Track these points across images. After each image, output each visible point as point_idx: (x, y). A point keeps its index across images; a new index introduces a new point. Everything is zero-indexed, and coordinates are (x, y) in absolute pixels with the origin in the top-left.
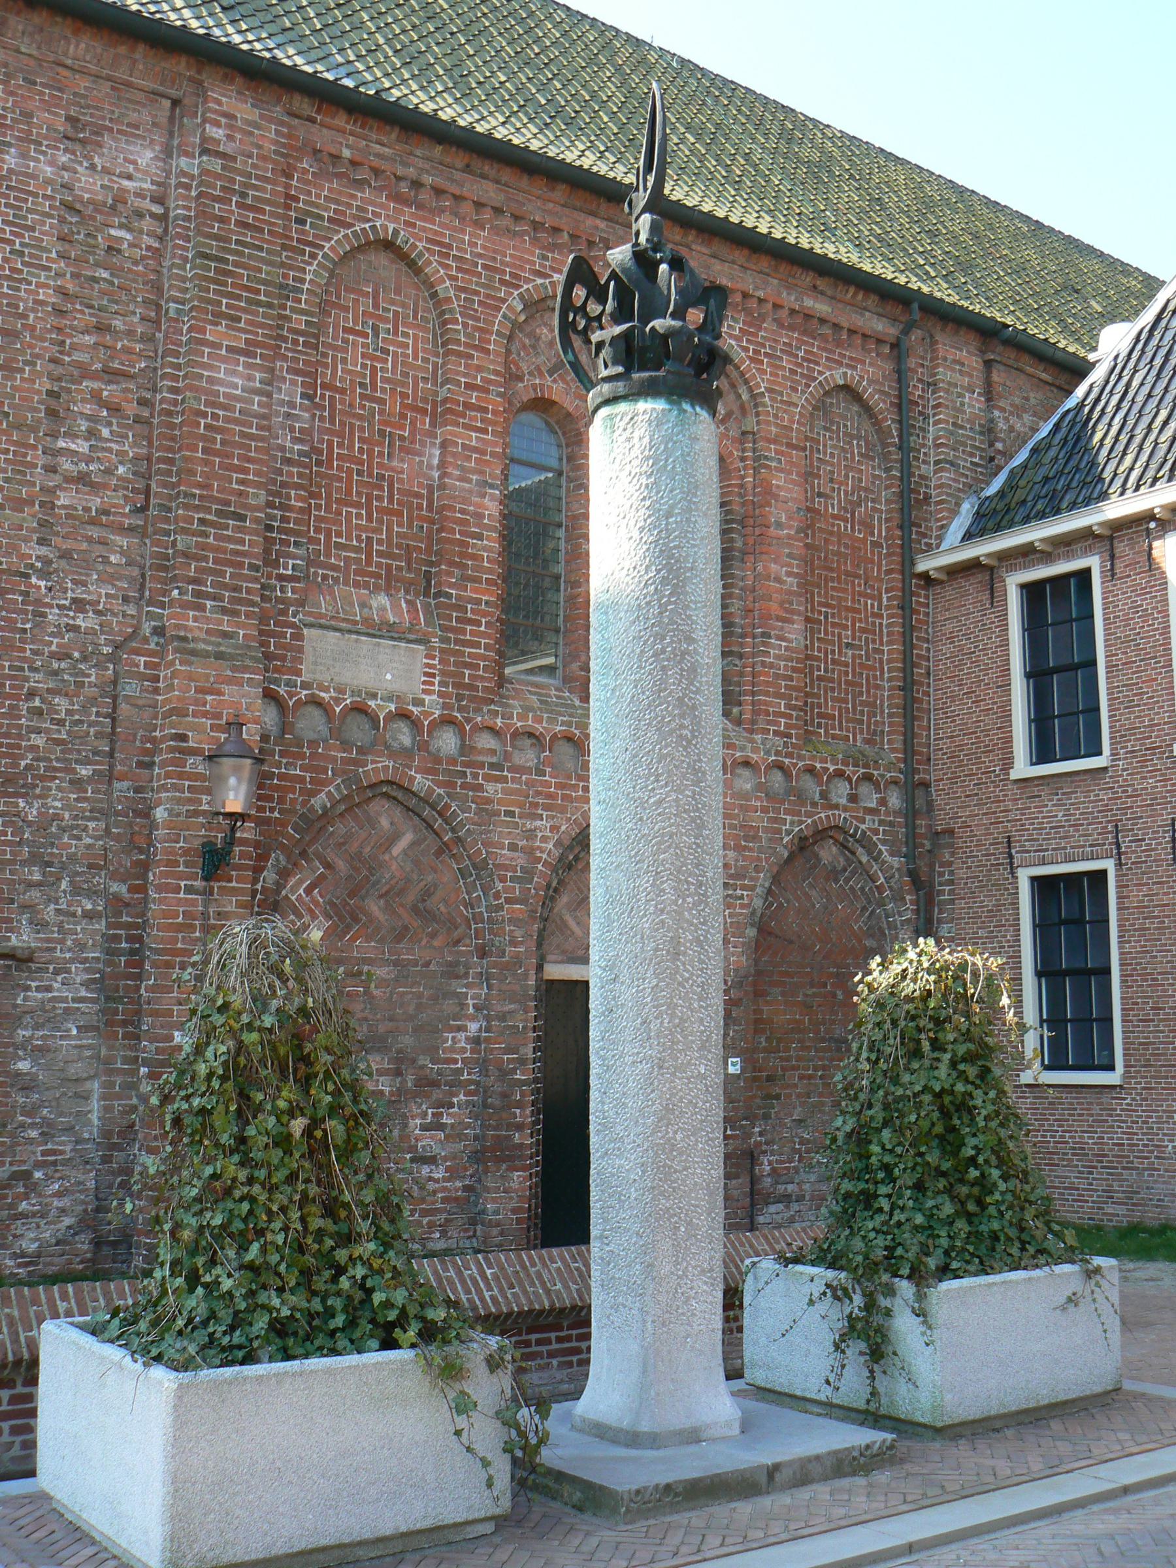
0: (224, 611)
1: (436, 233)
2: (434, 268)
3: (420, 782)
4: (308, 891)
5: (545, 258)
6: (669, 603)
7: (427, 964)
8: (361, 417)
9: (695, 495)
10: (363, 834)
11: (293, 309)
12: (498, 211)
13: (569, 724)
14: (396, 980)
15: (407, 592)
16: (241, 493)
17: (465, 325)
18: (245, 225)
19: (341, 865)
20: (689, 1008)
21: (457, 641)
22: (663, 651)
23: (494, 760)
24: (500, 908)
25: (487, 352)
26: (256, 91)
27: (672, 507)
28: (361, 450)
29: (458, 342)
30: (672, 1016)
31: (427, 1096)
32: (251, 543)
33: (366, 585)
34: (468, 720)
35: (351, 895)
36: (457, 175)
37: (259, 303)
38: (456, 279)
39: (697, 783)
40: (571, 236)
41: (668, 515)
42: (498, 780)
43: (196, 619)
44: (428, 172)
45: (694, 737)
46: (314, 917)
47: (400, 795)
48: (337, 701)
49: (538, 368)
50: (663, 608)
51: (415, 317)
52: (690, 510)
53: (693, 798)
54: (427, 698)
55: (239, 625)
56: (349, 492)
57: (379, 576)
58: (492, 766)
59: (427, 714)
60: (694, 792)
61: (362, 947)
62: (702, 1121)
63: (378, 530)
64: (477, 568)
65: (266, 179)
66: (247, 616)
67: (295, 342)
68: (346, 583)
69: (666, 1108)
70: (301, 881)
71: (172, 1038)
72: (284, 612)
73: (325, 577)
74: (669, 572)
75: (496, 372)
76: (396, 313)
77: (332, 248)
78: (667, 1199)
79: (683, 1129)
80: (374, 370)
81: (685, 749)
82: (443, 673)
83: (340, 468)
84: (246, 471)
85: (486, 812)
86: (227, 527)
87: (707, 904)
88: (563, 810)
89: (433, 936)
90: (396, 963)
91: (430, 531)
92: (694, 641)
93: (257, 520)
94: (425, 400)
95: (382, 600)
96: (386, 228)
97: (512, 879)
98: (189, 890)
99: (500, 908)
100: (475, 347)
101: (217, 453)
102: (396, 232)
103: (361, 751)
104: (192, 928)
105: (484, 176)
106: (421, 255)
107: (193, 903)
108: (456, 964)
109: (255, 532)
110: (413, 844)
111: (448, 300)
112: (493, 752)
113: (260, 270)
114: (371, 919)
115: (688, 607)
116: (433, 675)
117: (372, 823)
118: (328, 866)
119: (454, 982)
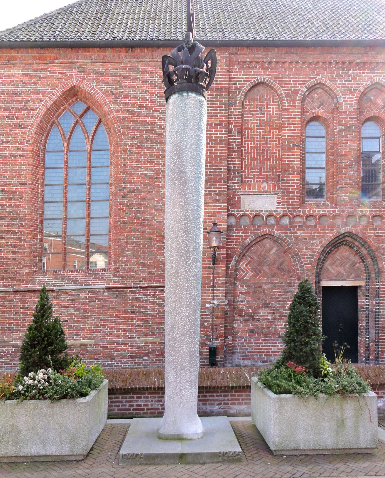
0: (217, 194)
1: (277, 75)
2: (277, 86)
3: (277, 233)
4: (246, 265)
5: (314, 73)
6: (177, 161)
7: (282, 283)
8: (257, 135)
9: (187, 123)
10: (261, 249)
11: (234, 109)
12: (297, 62)
13: (325, 211)
14: (272, 288)
15: (273, 181)
16: (220, 163)
17: (287, 100)
18: (218, 89)
19: (255, 257)
20: (182, 294)
21: (287, 192)
22: (175, 178)
23: (301, 225)
24: (303, 266)
25: (295, 106)
26: (220, 50)
27: (178, 130)
28: (257, 144)
29: (285, 106)
30: (176, 297)
31: (283, 319)
32: (224, 175)
33: (260, 181)
34: (291, 214)
35: (259, 266)
36: (283, 56)
37: (223, 110)
38: (284, 87)
39: (186, 219)
40: (323, 63)
41: (177, 132)
42: (301, 230)
43: (209, 198)
44: (274, 58)
45: (185, 205)
46: (248, 272)
47: (271, 237)
48: (238, 214)
49: (314, 108)
50: (175, 164)
51: (273, 102)
52: (184, 129)
53: (185, 224)
54: (278, 210)
55: (221, 198)
56: (254, 157)
57: (264, 178)
58: (299, 226)
59: (278, 214)
60: (185, 223)
61: (262, 280)
62: (187, 331)
63: (263, 165)
64: (294, 171)
65: (223, 75)
66: (223, 194)
67: (235, 118)
68: (254, 182)
69: (173, 327)
70: (244, 263)
71: (205, 305)
72: (235, 192)
73: (248, 181)
74: (177, 151)
75: (298, 112)
76: (267, 102)
77: (245, 89)
78: (173, 357)
79: (179, 334)
80: (260, 120)
81: (181, 209)
82: (283, 202)
83: (251, 150)
84: (221, 156)
85: (298, 239)
86: (217, 172)
87: (190, 259)
88: (323, 237)
89: (284, 275)
90: (272, 283)
91: (279, 163)
92: (186, 172)
93: (225, 169)
94: (276, 126)
95: (265, 184)
96: (261, 79)
97: (307, 258)
98: (209, 267)
99: (303, 266)
100: (291, 106)
101: (213, 153)
102: (264, 79)
103: (259, 226)
104: (210, 277)
105: (292, 54)
106: (273, 83)
107: (210, 271)
108: (291, 283)
109: (225, 172)
110: (277, 250)
111: (282, 94)
112: (300, 222)
113: (222, 101)
114: (265, 272)
115: (184, 162)
116: (280, 203)
117: (264, 246)
118: (251, 258)
119: (290, 288)
